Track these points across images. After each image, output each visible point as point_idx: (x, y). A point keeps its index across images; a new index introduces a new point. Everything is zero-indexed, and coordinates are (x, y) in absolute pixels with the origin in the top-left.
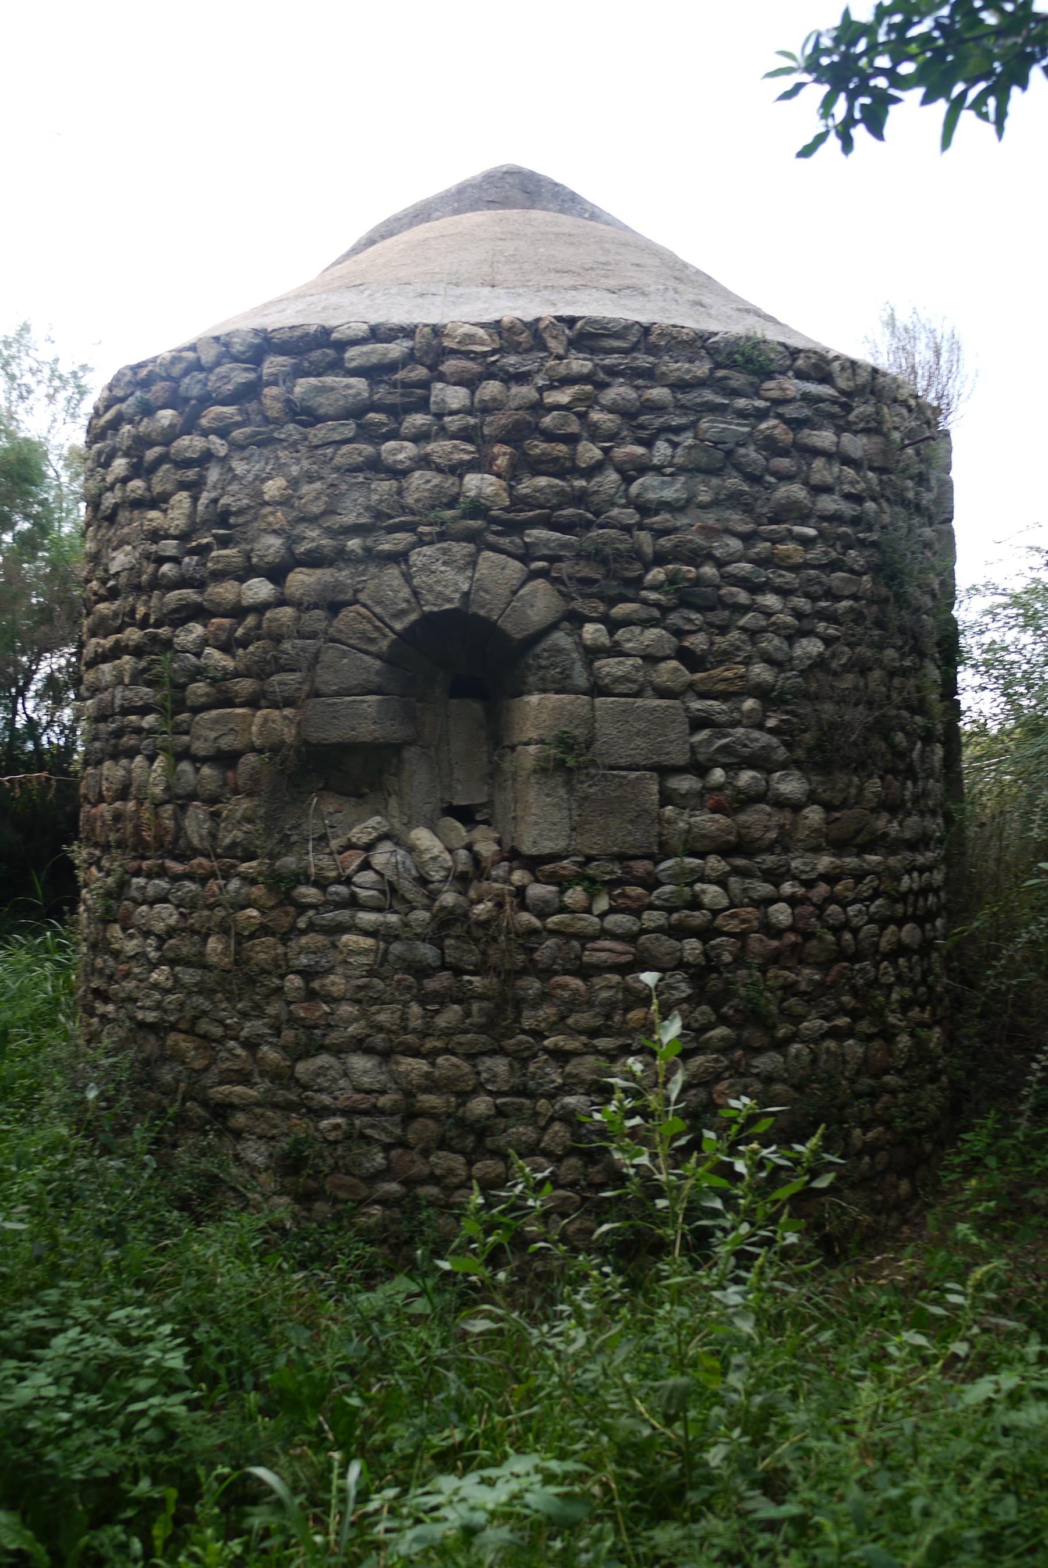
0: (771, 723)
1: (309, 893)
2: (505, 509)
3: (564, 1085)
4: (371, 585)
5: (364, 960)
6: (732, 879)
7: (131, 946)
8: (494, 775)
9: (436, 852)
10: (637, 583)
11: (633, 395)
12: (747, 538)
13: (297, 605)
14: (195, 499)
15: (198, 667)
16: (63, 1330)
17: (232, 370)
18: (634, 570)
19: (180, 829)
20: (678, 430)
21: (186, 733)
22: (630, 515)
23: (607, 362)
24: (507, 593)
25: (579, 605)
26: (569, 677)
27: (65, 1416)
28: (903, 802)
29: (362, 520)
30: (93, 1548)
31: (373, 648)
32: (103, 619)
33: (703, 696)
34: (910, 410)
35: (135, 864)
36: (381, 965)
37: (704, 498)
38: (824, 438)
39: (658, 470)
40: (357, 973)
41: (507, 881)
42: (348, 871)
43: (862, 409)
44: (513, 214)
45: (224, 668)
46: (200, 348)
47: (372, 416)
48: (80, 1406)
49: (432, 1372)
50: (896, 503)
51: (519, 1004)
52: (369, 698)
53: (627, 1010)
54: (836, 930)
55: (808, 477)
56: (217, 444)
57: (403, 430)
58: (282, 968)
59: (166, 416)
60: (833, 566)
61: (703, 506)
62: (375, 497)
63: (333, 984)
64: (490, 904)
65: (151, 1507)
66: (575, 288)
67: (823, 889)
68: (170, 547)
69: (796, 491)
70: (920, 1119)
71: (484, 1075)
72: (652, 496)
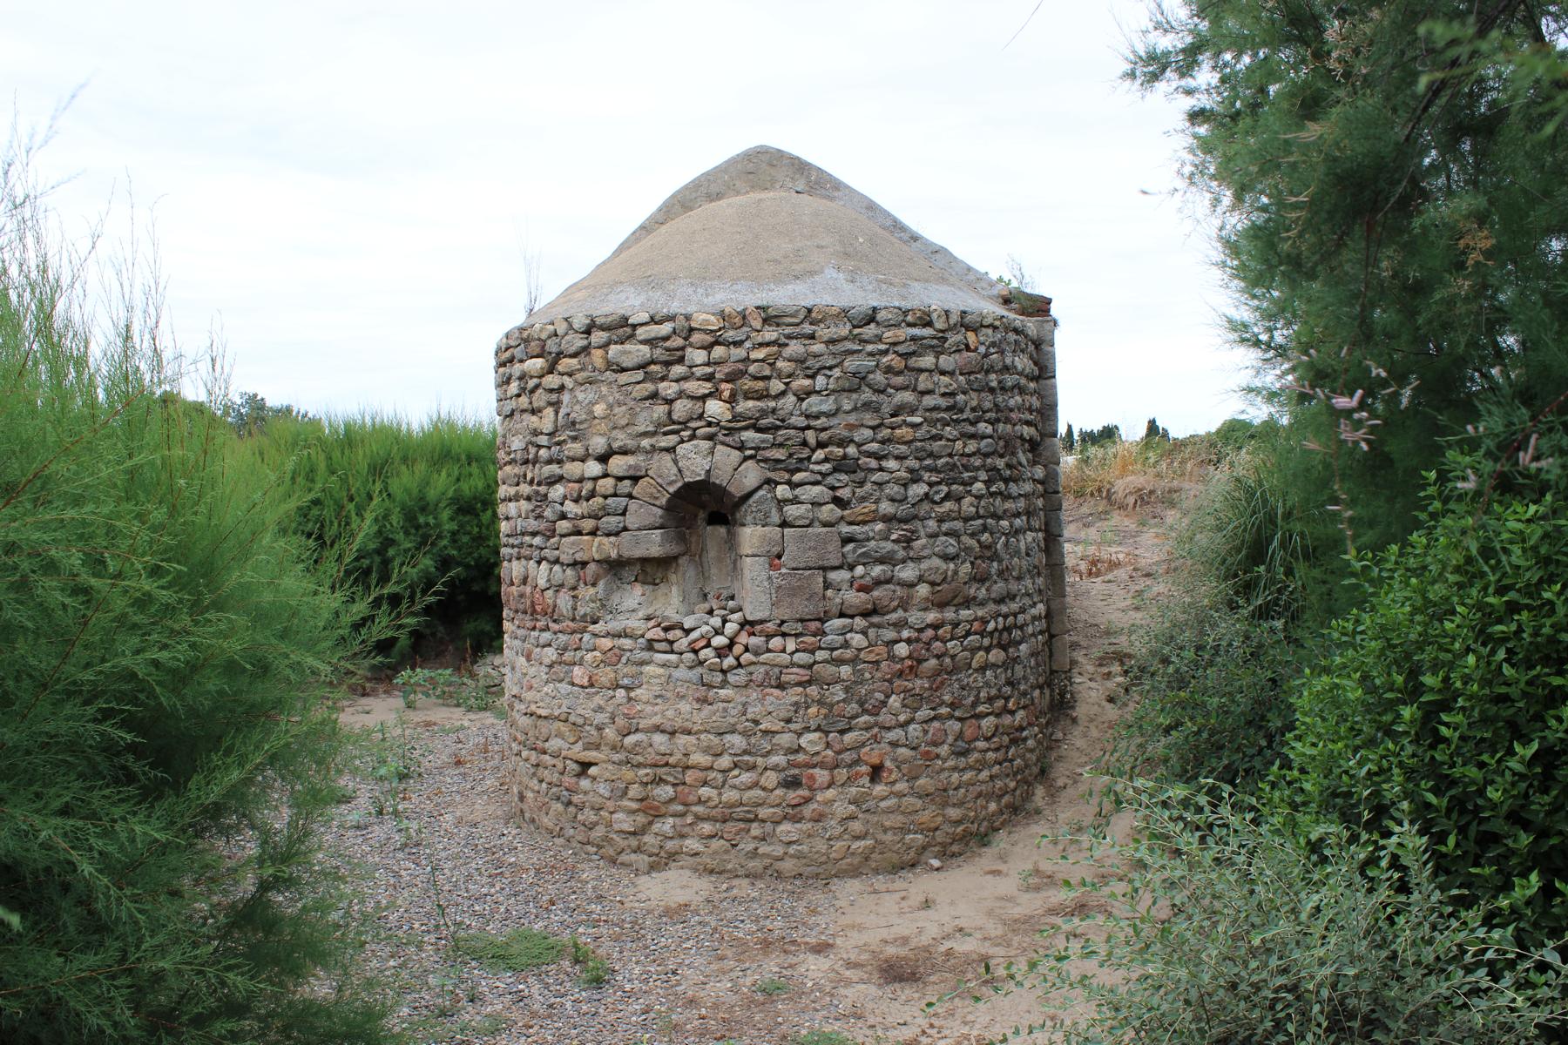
0: (894, 537)
2: (729, 421)
4: (655, 466)
5: (658, 681)
14: (557, 413)
20: (830, 368)
22: (802, 422)
31: (658, 503)
33: (851, 523)
37: (847, 407)
38: (927, 361)
43: (953, 338)
47: (652, 367)
55: (916, 385)
56: (568, 382)
57: (670, 376)
60: (938, 437)
67: (930, 633)
68: (543, 440)
69: (907, 397)
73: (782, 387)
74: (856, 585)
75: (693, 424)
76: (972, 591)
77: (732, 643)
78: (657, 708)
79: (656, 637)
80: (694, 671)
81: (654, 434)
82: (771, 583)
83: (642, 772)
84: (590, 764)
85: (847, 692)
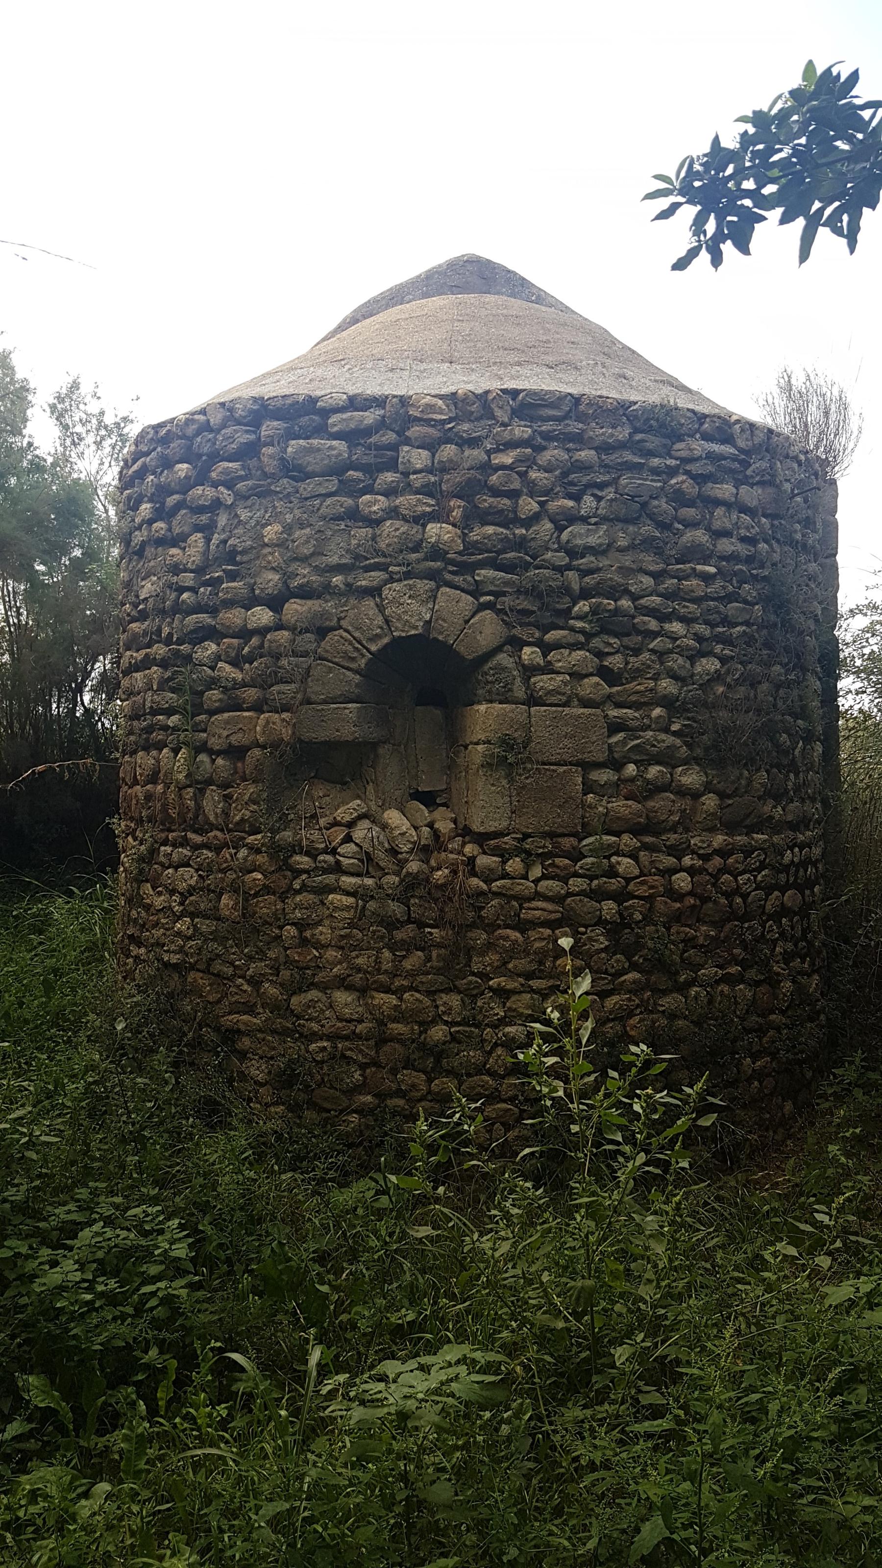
0: (675, 727)
1: (302, 861)
2: (460, 553)
3: (505, 1017)
4: (351, 613)
6: (642, 853)
7: (159, 902)
8: (451, 767)
9: (404, 829)
10: (567, 613)
12: (657, 576)
13: (292, 629)
14: (208, 540)
15: (212, 678)
16: (90, 1223)
17: (236, 431)
18: (564, 604)
19: (199, 807)
20: (602, 486)
21: (205, 731)
22: (562, 559)
23: (543, 428)
24: (461, 621)
25: (517, 631)
26: (511, 690)
27: (89, 1297)
28: (786, 791)
29: (344, 561)
30: (111, 1405)
31: (353, 666)
32: (135, 636)
33: (619, 705)
34: (800, 464)
35: (163, 835)
36: (360, 919)
38: (725, 490)
39: (584, 520)
40: (341, 925)
41: (460, 852)
42: (333, 844)
43: (758, 464)
44: (471, 298)
45: (234, 678)
46: (209, 412)
48: (100, 1288)
49: (393, 1259)
50: (785, 543)
51: (469, 952)
52: (350, 705)
54: (728, 895)
55: (710, 523)
56: (224, 493)
58: (280, 920)
59: (183, 469)
60: (729, 598)
61: (621, 550)
62: (354, 542)
63: (321, 933)
64: (446, 871)
65: (156, 1374)
66: (519, 364)
67: (717, 861)
68: (188, 579)
69: (700, 536)
70: (802, 1052)
71: (442, 1008)
72: (579, 542)
73: (535, 507)
76: (767, 809)
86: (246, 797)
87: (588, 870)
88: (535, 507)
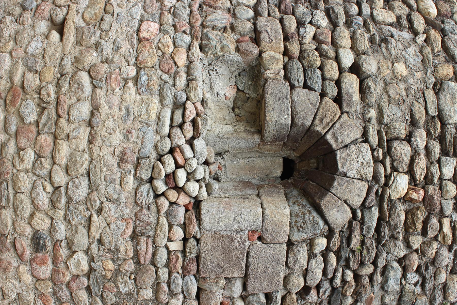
4: (351, 121)
5: (144, 112)
10: (347, 266)
11: (444, 264)
14: (392, 25)
20: (423, 286)
22: (381, 263)
24: (346, 198)
29: (385, 117)
31: (317, 122)
39: (404, 276)
47: (439, 125)
52: (290, 118)
53: (113, 260)
56: (421, 39)
74: (226, 301)
75: (388, 162)
77: (177, 188)
78: (116, 109)
79: (188, 113)
80: (152, 150)
81: (380, 121)
82: (237, 231)
83: (52, 89)
84: (61, 33)
85: (127, 294)
86: (225, 43)
87: (174, 281)
88: (415, 247)
